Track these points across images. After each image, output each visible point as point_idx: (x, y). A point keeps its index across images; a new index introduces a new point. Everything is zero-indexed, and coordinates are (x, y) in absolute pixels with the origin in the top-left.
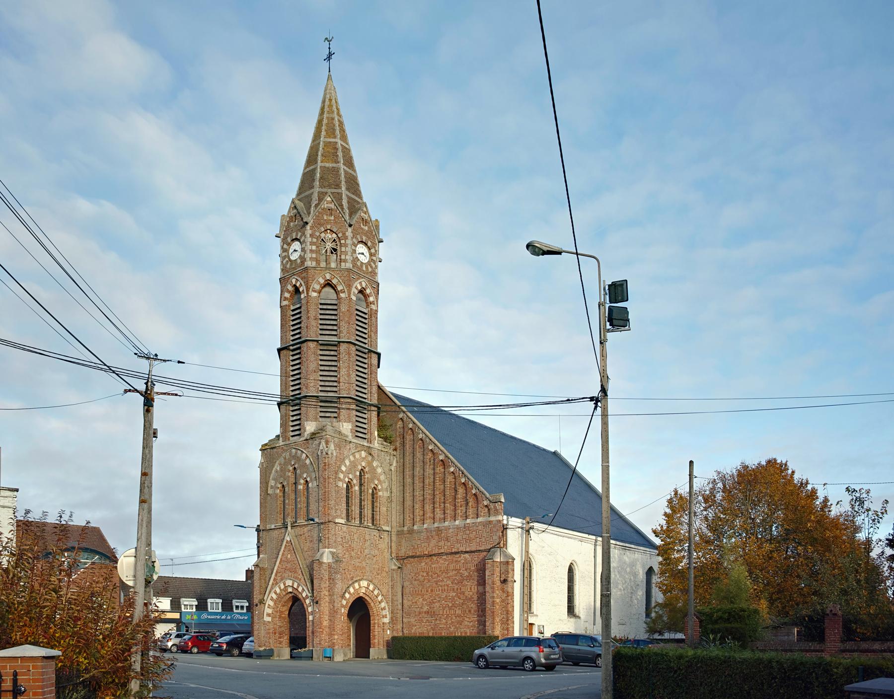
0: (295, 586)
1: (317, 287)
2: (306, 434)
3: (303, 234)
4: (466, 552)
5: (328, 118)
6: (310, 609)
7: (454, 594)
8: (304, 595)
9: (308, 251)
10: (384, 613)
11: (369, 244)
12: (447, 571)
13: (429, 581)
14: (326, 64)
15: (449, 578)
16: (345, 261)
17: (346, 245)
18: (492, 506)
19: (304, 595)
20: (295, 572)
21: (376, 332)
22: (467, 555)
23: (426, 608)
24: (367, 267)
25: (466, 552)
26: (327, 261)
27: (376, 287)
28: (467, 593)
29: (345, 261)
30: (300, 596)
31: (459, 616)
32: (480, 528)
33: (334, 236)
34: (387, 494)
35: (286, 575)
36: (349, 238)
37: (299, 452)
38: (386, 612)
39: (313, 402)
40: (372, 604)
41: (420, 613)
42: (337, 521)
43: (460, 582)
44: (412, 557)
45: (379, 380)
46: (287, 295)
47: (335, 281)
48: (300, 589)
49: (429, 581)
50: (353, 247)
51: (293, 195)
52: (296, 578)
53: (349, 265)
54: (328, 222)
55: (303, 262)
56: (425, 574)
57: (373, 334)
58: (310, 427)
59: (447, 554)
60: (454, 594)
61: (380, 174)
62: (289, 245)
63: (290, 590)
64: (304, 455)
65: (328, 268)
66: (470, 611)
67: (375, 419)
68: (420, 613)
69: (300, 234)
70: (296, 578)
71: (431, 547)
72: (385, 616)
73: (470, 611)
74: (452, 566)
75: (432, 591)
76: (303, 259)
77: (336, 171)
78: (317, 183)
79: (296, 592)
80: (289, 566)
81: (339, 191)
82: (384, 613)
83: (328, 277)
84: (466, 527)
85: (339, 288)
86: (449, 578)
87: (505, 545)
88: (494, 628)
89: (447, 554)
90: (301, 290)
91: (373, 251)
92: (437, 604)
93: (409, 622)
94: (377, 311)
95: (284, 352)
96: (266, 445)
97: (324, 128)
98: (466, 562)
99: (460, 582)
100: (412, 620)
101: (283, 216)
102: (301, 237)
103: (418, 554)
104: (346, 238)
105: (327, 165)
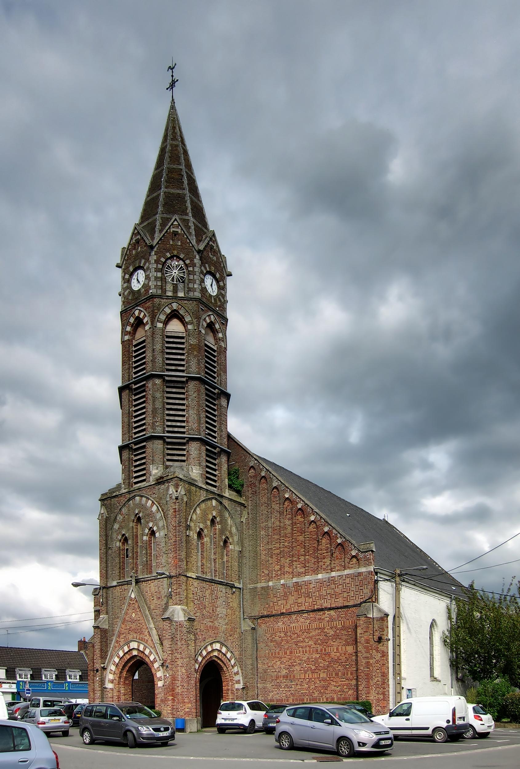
0: (141, 648)
1: (163, 317)
2: (151, 479)
3: (147, 260)
4: (330, 609)
5: (171, 145)
6: (159, 674)
7: (318, 656)
8: (152, 658)
9: (153, 279)
10: (236, 678)
11: (218, 276)
12: (308, 631)
13: (287, 642)
14: (169, 93)
15: (311, 638)
16: (194, 290)
17: (193, 273)
18: (361, 555)
19: (152, 658)
20: (141, 633)
21: (225, 372)
22: (332, 612)
23: (284, 672)
24: (215, 300)
25: (330, 609)
26: (175, 290)
27: (224, 320)
28: (333, 655)
29: (194, 290)
30: (147, 660)
31: (324, 680)
32: (347, 581)
33: (181, 262)
34: (238, 548)
35: (130, 637)
36: (198, 265)
37: (144, 499)
38: (239, 677)
39: (158, 445)
40: (225, 668)
41: (277, 677)
42: (189, 575)
43: (324, 642)
44: (268, 616)
45: (229, 430)
46: (129, 329)
47: (182, 312)
48: (147, 652)
49: (287, 642)
50: (202, 276)
51: (137, 219)
52: (142, 639)
53: (197, 294)
54: (174, 247)
55: (147, 291)
56: (282, 635)
57: (222, 374)
58: (155, 471)
59: (308, 612)
60: (318, 656)
61: (228, 199)
62: (131, 275)
63: (135, 653)
64: (150, 502)
65: (175, 298)
66: (337, 674)
67: (225, 467)
68: (277, 677)
69: (143, 261)
70: (142, 639)
71: (290, 604)
72: (238, 682)
73: (337, 674)
74: (314, 625)
75: (291, 653)
76: (146, 287)
77: (181, 198)
78: (160, 209)
79: (142, 655)
80: (133, 626)
81: (187, 218)
82: (236, 678)
83: (175, 306)
84: (332, 580)
85: (188, 319)
86: (311, 638)
87: (377, 600)
88: (369, 693)
89: (308, 612)
90: (145, 321)
91: (221, 284)
92: (298, 668)
93: (264, 688)
94: (226, 348)
95: (126, 393)
96: (106, 494)
97: (167, 155)
98: (332, 619)
99: (324, 642)
100: (269, 685)
101: (124, 248)
102: (145, 264)
103: (274, 612)
104: (194, 265)
105: (172, 191)
